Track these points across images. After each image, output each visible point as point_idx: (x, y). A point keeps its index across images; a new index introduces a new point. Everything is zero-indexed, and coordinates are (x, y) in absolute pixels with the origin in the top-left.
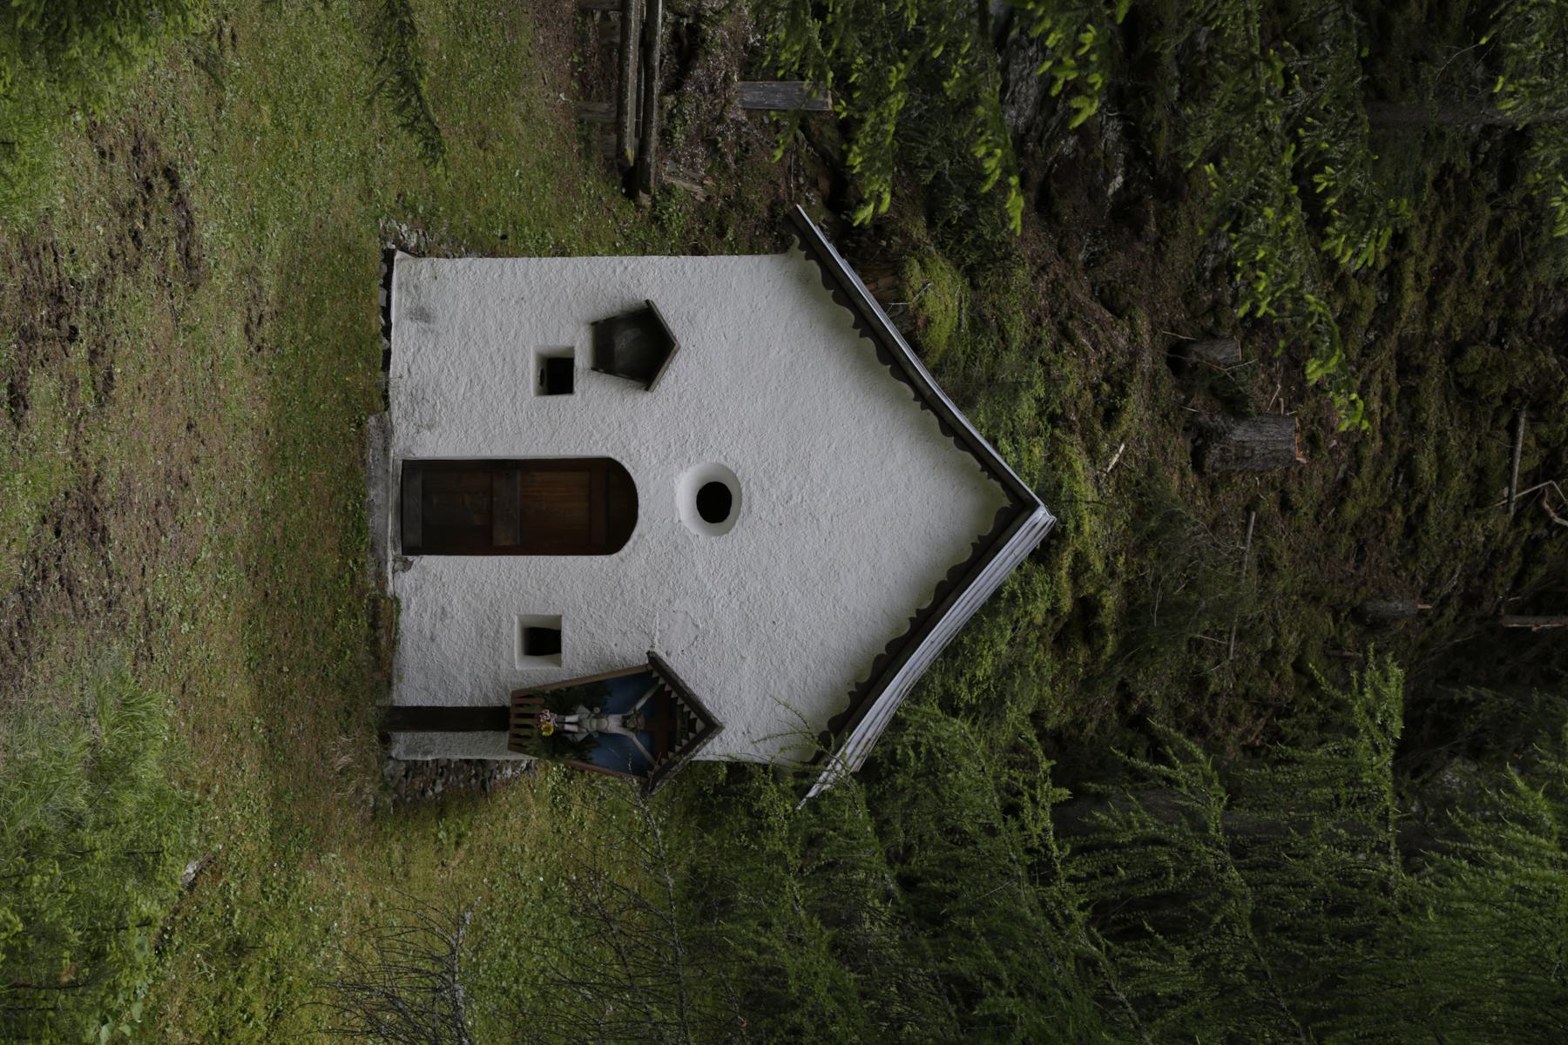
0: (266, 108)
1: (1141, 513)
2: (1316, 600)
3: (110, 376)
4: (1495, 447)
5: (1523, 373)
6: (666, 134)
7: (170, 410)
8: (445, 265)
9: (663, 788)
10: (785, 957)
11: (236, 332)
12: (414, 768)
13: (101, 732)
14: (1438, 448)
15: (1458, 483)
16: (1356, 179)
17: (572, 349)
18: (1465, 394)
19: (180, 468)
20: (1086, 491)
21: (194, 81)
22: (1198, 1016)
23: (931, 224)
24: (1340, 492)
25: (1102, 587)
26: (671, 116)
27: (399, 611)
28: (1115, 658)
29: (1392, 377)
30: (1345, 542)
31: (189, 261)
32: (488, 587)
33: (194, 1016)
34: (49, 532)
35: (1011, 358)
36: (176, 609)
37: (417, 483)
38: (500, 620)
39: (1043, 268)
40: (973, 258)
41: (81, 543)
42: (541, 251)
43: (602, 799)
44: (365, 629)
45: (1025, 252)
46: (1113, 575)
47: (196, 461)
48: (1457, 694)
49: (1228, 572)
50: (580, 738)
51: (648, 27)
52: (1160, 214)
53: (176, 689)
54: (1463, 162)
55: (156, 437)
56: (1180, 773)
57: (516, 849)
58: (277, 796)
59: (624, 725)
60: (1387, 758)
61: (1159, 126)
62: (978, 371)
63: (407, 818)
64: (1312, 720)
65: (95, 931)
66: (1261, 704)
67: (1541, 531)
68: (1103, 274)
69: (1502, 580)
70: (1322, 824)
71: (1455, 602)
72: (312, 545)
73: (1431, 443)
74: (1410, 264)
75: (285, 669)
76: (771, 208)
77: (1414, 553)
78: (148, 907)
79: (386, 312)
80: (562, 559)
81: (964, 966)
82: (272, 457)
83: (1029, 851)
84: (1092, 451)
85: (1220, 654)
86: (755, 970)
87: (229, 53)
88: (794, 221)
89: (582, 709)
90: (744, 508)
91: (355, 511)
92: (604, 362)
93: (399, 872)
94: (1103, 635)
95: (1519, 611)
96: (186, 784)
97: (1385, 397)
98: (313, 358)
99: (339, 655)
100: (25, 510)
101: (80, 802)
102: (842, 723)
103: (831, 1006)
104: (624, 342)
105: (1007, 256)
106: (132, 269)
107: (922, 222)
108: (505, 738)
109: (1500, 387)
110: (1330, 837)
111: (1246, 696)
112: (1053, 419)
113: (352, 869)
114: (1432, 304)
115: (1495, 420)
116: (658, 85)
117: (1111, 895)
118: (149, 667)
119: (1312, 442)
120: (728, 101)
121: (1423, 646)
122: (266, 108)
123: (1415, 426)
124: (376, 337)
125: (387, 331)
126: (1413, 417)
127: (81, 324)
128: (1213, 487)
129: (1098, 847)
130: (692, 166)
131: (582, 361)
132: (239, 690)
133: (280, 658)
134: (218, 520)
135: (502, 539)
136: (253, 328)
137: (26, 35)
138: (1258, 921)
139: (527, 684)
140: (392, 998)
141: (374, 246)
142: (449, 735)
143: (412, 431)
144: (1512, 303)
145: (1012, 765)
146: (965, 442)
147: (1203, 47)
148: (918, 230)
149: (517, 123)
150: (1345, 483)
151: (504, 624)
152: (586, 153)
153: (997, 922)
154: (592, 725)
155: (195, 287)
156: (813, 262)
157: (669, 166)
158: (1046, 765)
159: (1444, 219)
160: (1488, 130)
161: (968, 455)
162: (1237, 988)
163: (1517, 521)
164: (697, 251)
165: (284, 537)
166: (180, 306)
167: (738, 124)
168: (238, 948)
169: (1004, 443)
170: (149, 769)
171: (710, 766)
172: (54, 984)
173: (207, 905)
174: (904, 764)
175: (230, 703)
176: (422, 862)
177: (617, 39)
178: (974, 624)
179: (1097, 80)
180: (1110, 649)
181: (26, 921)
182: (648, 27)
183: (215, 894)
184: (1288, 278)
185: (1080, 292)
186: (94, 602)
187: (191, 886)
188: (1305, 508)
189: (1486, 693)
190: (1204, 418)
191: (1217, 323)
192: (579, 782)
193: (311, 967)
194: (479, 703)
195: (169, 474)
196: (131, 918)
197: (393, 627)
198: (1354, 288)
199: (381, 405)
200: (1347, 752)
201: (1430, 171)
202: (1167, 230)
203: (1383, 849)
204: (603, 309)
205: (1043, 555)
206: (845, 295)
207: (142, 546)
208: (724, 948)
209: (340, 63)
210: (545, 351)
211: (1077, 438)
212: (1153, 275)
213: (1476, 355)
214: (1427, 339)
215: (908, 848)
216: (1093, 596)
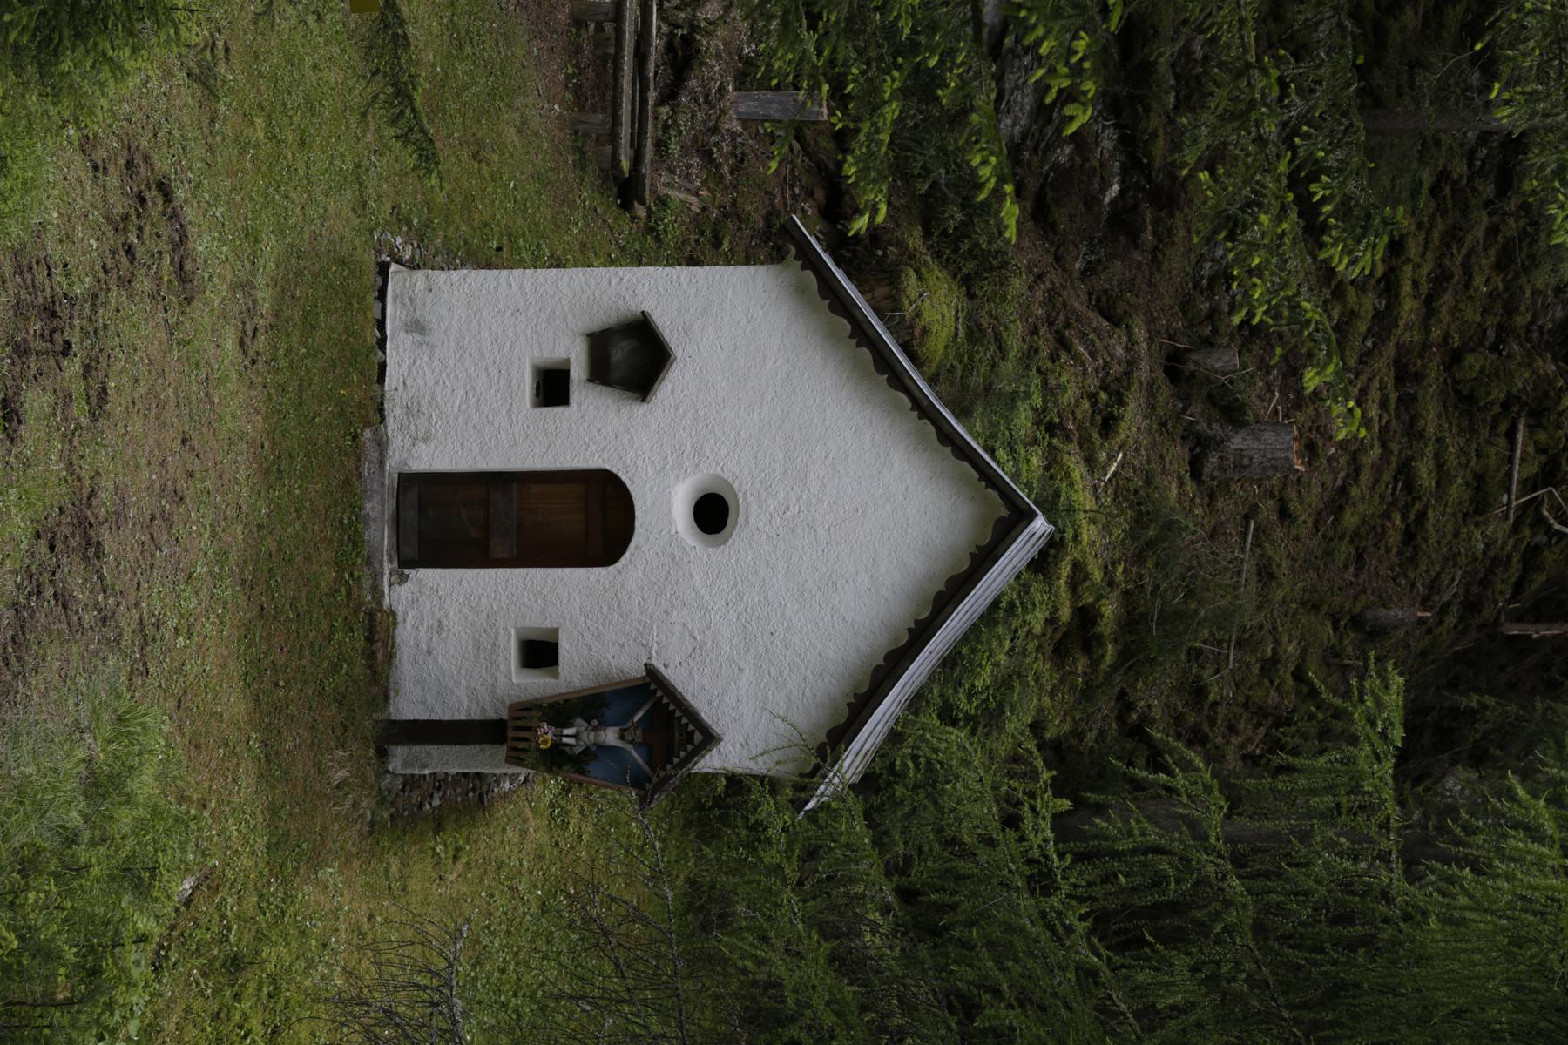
0: (259, 121)
6: (661, 145)
7: (165, 424)
12: (411, 782)
14: (1437, 456)
15: (1456, 490)
17: (567, 361)
18: (1463, 400)
19: (175, 481)
24: (1338, 500)
27: (395, 624)
32: (484, 600)
37: (413, 495)
43: (600, 811)
44: (361, 643)
46: (1111, 583)
47: (191, 475)
50: (578, 750)
52: (1156, 222)
55: (151, 451)
57: (514, 862)
59: (622, 738)
61: (1154, 135)
68: (1100, 283)
73: (1429, 450)
75: (282, 683)
77: (1413, 560)
82: (267, 471)
89: (580, 721)
90: (741, 519)
91: (350, 523)
92: (600, 373)
94: (1102, 644)
97: (1384, 405)
98: (308, 371)
99: (336, 668)
104: (620, 353)
109: (1497, 394)
111: (1246, 705)
115: (1494, 427)
120: (723, 112)
123: (1413, 433)
125: (382, 343)
130: (688, 176)
131: (578, 372)
132: (235, 705)
133: (276, 672)
134: (213, 534)
136: (248, 341)
142: (447, 748)
143: (408, 443)
147: (1199, 55)
150: (1343, 490)
151: (501, 637)
165: (280, 550)
166: (175, 320)
168: (235, 964)
175: (226, 717)
177: (612, 50)
183: (212, 910)
186: (89, 618)
187: (188, 902)
190: (1202, 426)
191: (1215, 331)
192: (577, 795)
195: (163, 488)
197: (390, 640)
199: (376, 418)
202: (1164, 238)
207: (137, 561)
213: (1474, 362)
214: (1426, 346)
216: (1092, 605)
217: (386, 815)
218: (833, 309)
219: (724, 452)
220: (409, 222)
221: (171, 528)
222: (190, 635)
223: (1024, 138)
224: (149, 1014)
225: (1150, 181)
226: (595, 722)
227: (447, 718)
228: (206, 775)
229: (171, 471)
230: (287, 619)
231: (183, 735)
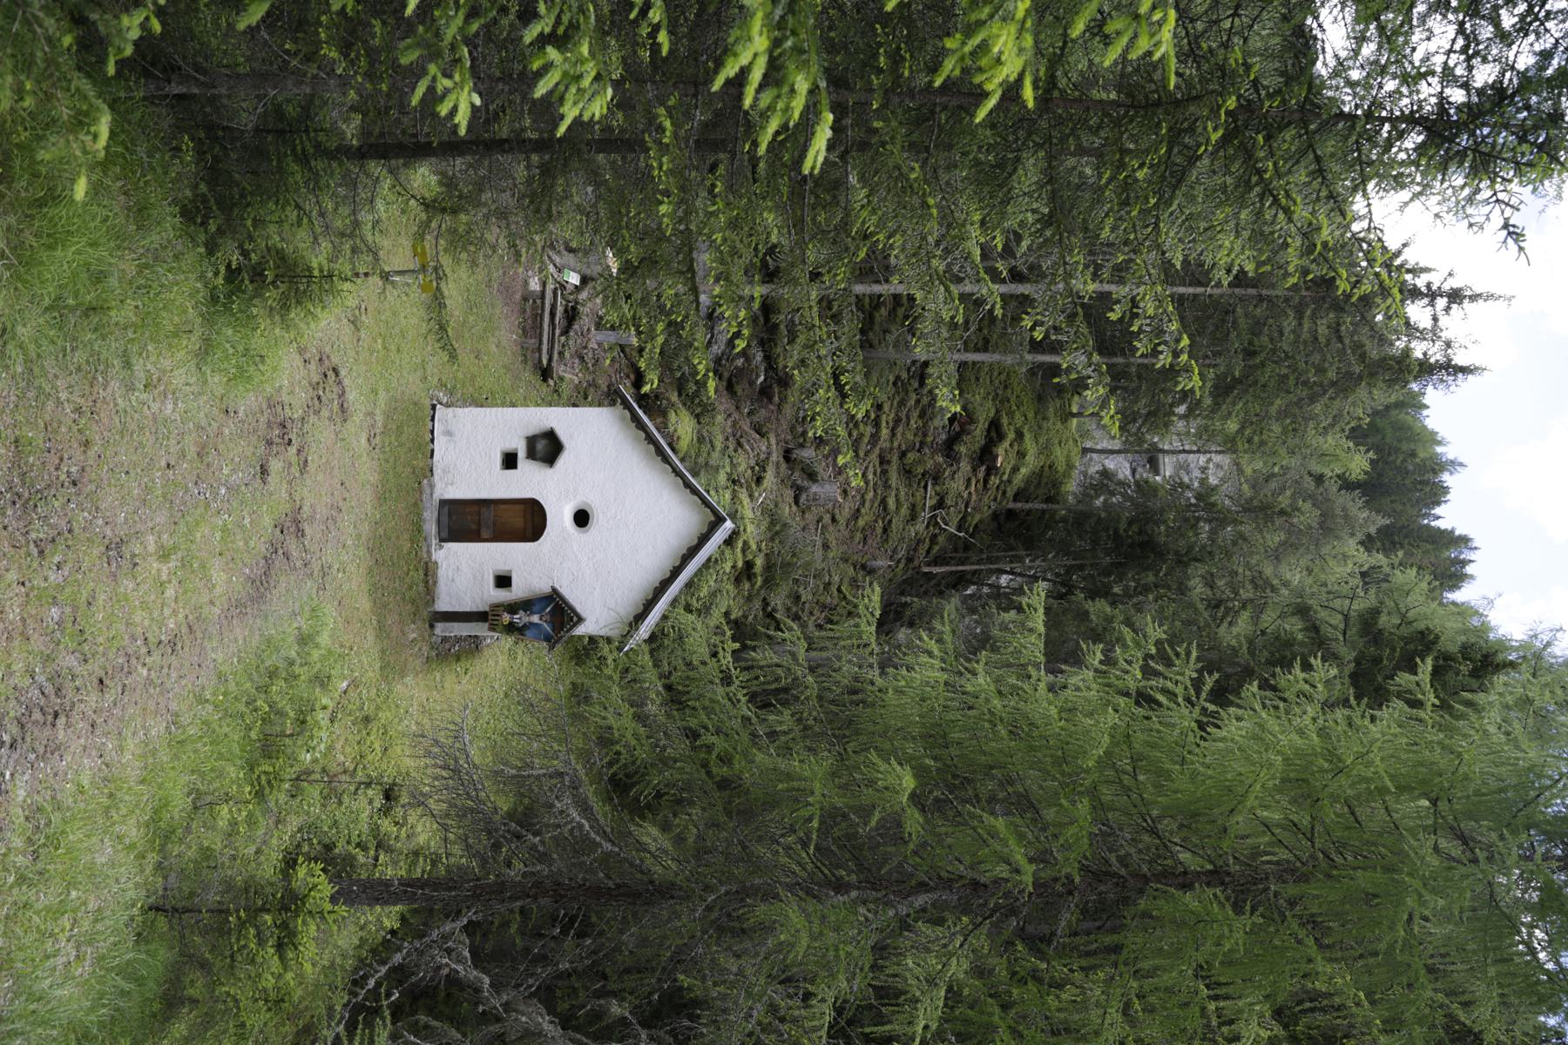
0: (379, 341)
1: (772, 523)
2: (847, 561)
3: (306, 461)
4: (919, 495)
5: (930, 464)
8: (459, 411)
9: (559, 647)
10: (612, 721)
11: (363, 440)
12: (445, 639)
13: (302, 622)
15: (904, 511)
16: (858, 378)
18: (907, 472)
20: (748, 513)
21: (347, 329)
22: (793, 739)
23: (680, 395)
24: (856, 514)
26: (563, 346)
28: (761, 587)
29: (877, 464)
30: (859, 536)
33: (348, 750)
34: (278, 531)
35: (716, 455)
36: (336, 567)
37: (446, 509)
39: (729, 415)
40: (698, 410)
41: (293, 537)
42: (503, 405)
44: (422, 577)
45: (721, 408)
46: (760, 550)
48: (903, 599)
49: (810, 549)
51: (553, 307)
52: (780, 393)
53: (336, 603)
54: (904, 375)
56: (787, 635)
58: (383, 651)
60: (873, 628)
61: (779, 355)
62: (701, 460)
64: (845, 613)
65: (302, 712)
66: (824, 607)
67: (937, 531)
68: (755, 418)
69: (922, 551)
70: (846, 657)
71: (903, 561)
72: (398, 538)
73: (893, 494)
74: (884, 417)
76: (609, 387)
77: (886, 540)
78: (325, 701)
79: (432, 432)
81: (693, 723)
83: (722, 672)
84: (751, 496)
85: (806, 585)
86: (601, 727)
87: (363, 318)
88: (618, 393)
92: (532, 454)
93: (439, 686)
95: (928, 565)
96: (342, 646)
97: (875, 474)
99: (410, 588)
100: (267, 521)
101: (293, 654)
102: (640, 617)
103: (633, 742)
104: (541, 446)
105: (714, 409)
106: (317, 413)
107: (676, 394)
108: (486, 625)
109: (920, 470)
110: (850, 662)
112: (734, 482)
113: (417, 684)
114: (893, 435)
116: (558, 332)
117: (758, 689)
119: (845, 492)
121: (890, 580)
122: (379, 341)
123: (887, 486)
125: (432, 441)
126: (886, 482)
127: (294, 438)
128: (803, 512)
129: (752, 667)
131: (522, 454)
132: (365, 604)
135: (485, 535)
137: (271, 309)
138: (820, 698)
140: (436, 742)
141: (427, 403)
144: (925, 435)
145: (715, 634)
146: (695, 491)
148: (674, 397)
149: (493, 348)
150: (858, 510)
152: (525, 361)
153: (707, 703)
154: (526, 619)
155: (345, 421)
157: (563, 368)
158: (729, 633)
159: (897, 399)
160: (914, 362)
162: (811, 727)
163: (927, 527)
164: (575, 405)
167: (594, 350)
168: (367, 719)
169: (712, 493)
170: (324, 639)
171: (580, 638)
172: (283, 735)
174: (668, 635)
176: (450, 680)
178: (699, 573)
179: (746, 332)
180: (759, 584)
181: (270, 706)
182: (553, 307)
184: (829, 420)
185: (746, 425)
187: (345, 692)
188: (842, 521)
189: (915, 599)
190: (799, 482)
194: (475, 609)
196: (317, 707)
197: (435, 575)
198: (861, 426)
200: (857, 626)
201: (892, 379)
202: (783, 400)
203: (871, 666)
204: (532, 431)
205: (729, 542)
206: (640, 425)
208: (585, 718)
209: (414, 321)
211: (744, 490)
213: (911, 456)
214: (892, 449)
215: (670, 673)
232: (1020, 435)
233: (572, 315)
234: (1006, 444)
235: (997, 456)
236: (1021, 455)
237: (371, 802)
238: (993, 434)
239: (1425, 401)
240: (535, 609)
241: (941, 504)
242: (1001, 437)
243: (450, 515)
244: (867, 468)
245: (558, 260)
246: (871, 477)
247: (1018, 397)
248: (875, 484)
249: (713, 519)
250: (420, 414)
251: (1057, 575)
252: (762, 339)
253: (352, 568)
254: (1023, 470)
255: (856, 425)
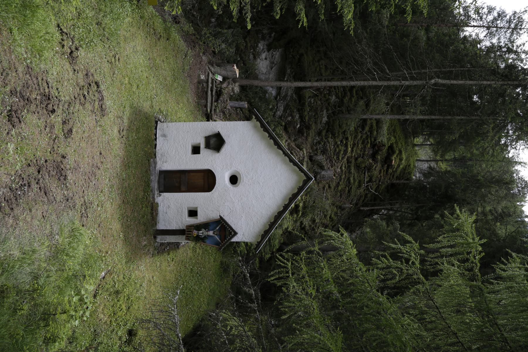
0: (127, 79)
6: (215, 110)
7: (94, 147)
11: (116, 131)
12: (162, 244)
14: (353, 177)
15: (356, 183)
17: (200, 144)
18: (358, 167)
19: (97, 164)
24: (338, 184)
25: (300, 202)
27: (158, 206)
30: (339, 194)
31: (102, 108)
32: (180, 200)
37: (162, 176)
38: (183, 208)
43: (203, 248)
44: (150, 211)
46: (302, 200)
47: (102, 162)
50: (203, 237)
51: (212, 88)
52: (306, 132)
55: (89, 153)
57: (185, 261)
59: (214, 233)
61: (306, 116)
63: (160, 256)
68: (297, 143)
72: (136, 189)
73: (352, 176)
75: (129, 220)
77: (349, 196)
79: (156, 135)
80: (198, 193)
82: (125, 166)
89: (203, 230)
90: (242, 181)
91: (147, 181)
92: (208, 146)
94: (299, 212)
97: (345, 167)
98: (137, 142)
99: (143, 217)
104: (212, 141)
108: (184, 237)
109: (363, 166)
111: (321, 223)
114: (352, 151)
115: (362, 172)
118: (86, 220)
120: (227, 105)
123: (350, 173)
124: (153, 140)
125: (156, 139)
126: (350, 171)
128: (318, 183)
130: (220, 117)
131: (202, 146)
132: (116, 226)
133: (128, 218)
134: (109, 180)
135: (183, 189)
136: (121, 131)
139: (189, 224)
142: (171, 236)
143: (162, 163)
144: (365, 151)
146: (295, 164)
147: (312, 102)
150: (339, 183)
151: (184, 209)
156: (258, 122)
161: (296, 167)
163: (364, 190)
165: (129, 186)
166: (98, 119)
168: (117, 292)
173: (108, 283)
175: (113, 229)
177: (206, 90)
182: (212, 88)
183: (110, 279)
185: (293, 145)
187: (104, 278)
190: (316, 170)
191: (317, 152)
192: (198, 245)
193: (137, 295)
195: (93, 165)
197: (157, 210)
198: (340, 146)
199: (154, 157)
202: (308, 135)
204: (207, 134)
207: (83, 184)
210: (193, 144)
212: (306, 143)
213: (360, 160)
214: (352, 157)
216: (298, 204)
217: (156, 252)
218: (264, 130)
219: (237, 165)
220: (163, 113)
221: (95, 176)
222: (102, 207)
223: (282, 115)
224: (94, 308)
225: (305, 124)
226: (207, 230)
227: (170, 229)
228: (108, 245)
229: (96, 161)
230: (131, 204)
231: (100, 234)
232: (400, 152)
233: (219, 94)
234: (395, 156)
235: (392, 160)
236: (401, 160)
237: (120, 339)
238: (390, 151)
239: (219, 217)
240: (211, 228)
241: (370, 181)
242: (394, 152)
243: (165, 179)
244: (342, 165)
245: (213, 69)
246: (344, 168)
247: (399, 136)
248: (345, 172)
249: (305, 178)
250: (149, 124)
251: (412, 210)
252: (299, 109)
253: (108, 205)
254: (401, 166)
255: (338, 146)
